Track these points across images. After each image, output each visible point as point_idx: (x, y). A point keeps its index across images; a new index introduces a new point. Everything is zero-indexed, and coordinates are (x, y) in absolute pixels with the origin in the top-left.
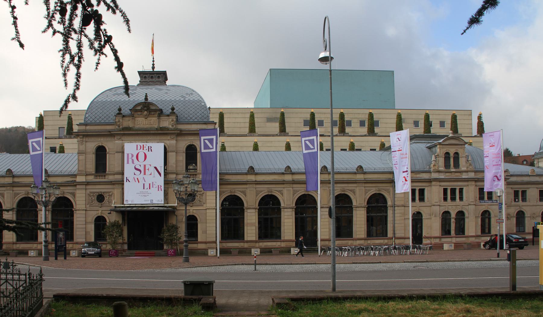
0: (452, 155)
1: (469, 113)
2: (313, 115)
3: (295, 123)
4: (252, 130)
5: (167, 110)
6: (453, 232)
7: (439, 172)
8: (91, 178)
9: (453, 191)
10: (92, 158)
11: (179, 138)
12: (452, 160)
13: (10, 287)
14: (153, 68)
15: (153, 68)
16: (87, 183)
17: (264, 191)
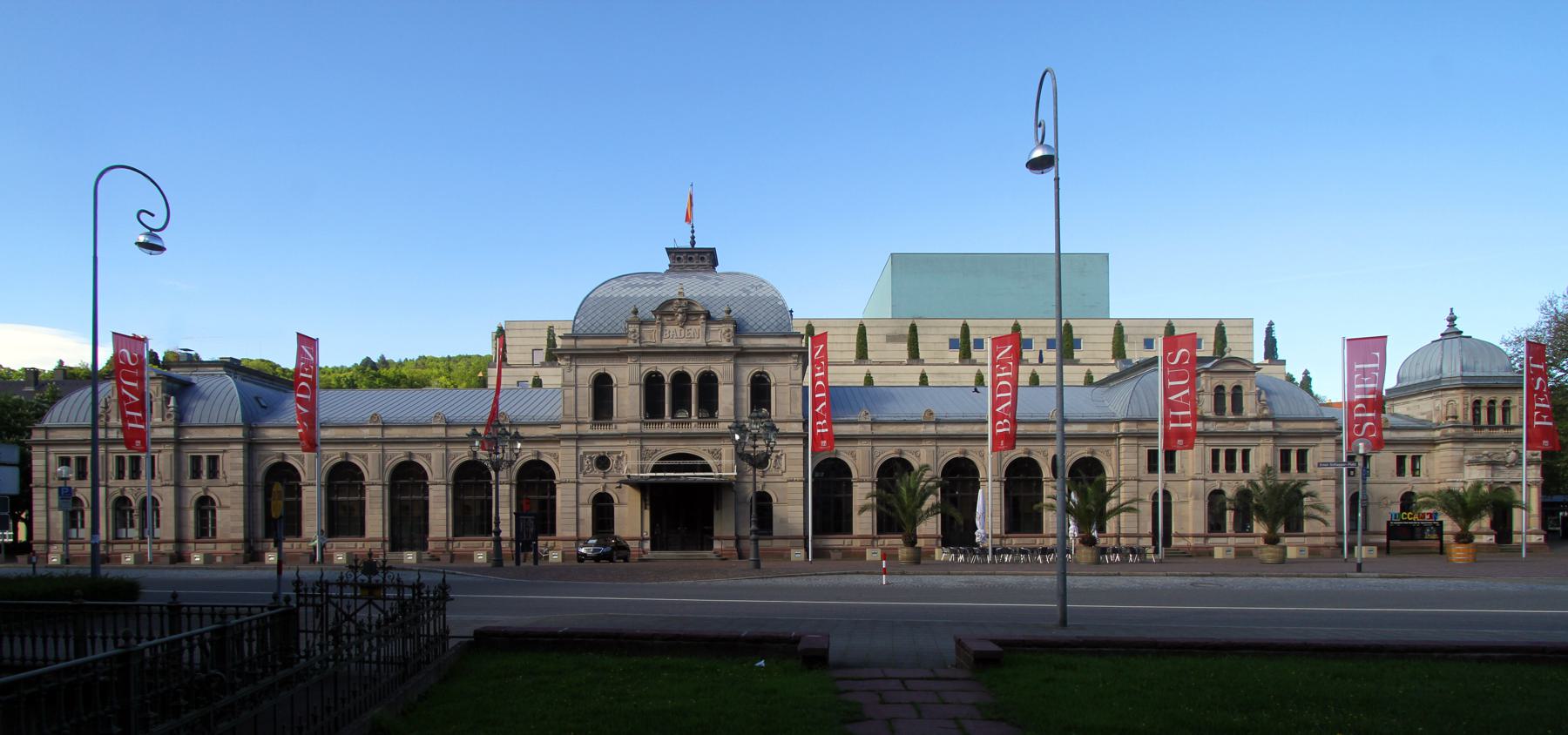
0: (1228, 390)
1: (1248, 324)
2: (965, 330)
3: (934, 343)
4: (862, 354)
5: (719, 313)
6: (1229, 527)
7: (1205, 419)
8: (586, 429)
9: (1230, 455)
10: (586, 393)
11: (740, 361)
12: (1228, 400)
13: (376, 615)
14: (693, 243)
15: (693, 243)
16: (580, 438)
17: (398, 454)
